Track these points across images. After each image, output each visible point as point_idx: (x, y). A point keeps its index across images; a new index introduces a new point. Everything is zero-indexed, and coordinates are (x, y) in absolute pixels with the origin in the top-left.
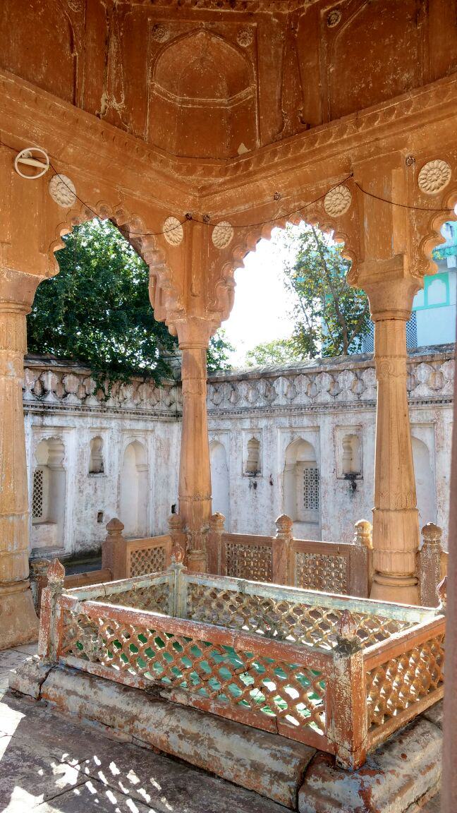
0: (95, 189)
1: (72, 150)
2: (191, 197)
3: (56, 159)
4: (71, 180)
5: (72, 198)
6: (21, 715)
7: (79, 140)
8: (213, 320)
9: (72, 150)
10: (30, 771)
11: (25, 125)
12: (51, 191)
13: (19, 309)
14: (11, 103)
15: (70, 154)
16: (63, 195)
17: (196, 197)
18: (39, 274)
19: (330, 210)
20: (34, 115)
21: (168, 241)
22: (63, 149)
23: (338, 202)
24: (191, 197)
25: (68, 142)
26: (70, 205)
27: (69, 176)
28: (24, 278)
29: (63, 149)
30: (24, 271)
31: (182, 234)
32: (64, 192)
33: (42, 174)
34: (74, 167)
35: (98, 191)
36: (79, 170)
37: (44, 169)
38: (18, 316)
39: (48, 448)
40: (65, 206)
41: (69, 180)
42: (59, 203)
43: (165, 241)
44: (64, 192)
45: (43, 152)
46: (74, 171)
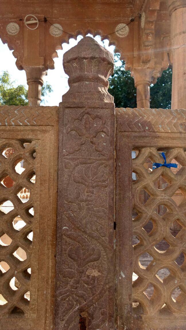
0: (74, 25)
2: (129, 9)
4: (60, 24)
5: (61, 32)
8: (148, 68)
9: (56, 11)
10: (47, 326)
12: (50, 32)
16: (12, 30)
17: (132, 7)
18: (39, 66)
19: (8, 29)
21: (119, 36)
23: (13, 29)
24: (129, 9)
26: (59, 35)
28: (33, 69)
31: (128, 30)
35: (75, 25)
36: (64, 19)
40: (57, 36)
41: (59, 25)
42: (54, 36)
43: (117, 36)
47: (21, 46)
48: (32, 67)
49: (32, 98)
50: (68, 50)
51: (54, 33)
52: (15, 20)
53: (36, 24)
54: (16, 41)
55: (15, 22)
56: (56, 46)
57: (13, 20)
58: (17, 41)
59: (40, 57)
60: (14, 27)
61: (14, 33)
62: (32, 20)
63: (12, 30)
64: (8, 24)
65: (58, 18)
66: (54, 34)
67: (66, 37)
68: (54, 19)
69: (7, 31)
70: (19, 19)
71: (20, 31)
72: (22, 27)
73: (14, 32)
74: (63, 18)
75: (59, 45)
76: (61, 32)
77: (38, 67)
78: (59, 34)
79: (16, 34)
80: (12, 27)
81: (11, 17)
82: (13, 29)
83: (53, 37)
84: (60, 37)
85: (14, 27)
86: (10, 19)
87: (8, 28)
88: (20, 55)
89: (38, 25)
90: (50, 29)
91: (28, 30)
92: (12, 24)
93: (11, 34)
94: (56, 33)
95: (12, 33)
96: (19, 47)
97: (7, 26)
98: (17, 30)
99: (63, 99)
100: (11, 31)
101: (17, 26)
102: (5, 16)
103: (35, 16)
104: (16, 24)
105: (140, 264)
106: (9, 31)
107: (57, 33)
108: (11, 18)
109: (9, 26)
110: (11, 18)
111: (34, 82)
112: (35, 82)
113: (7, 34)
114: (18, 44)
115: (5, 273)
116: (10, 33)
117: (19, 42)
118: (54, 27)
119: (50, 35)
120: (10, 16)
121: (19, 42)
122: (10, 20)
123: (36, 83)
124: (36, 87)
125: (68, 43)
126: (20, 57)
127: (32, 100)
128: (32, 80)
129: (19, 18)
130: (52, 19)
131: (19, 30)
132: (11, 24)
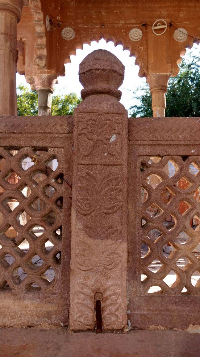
1: (182, 15)
3: (176, 22)
4: (185, 29)
5: (185, 37)
6: (65, 65)
7: (184, 9)
11: (158, 13)
12: (174, 37)
13: (159, 89)
14: (149, 7)
15: (182, 17)
18: (167, 73)
20: (160, 7)
22: (178, 16)
23: (136, 35)
25: (179, 12)
26: (184, 40)
27: (183, 27)
28: (160, 76)
29: (178, 16)
30: (160, 73)
32: (181, 35)
33: (165, 30)
34: (186, 22)
36: (189, 22)
37: (154, 27)
38: (159, 92)
39: (138, 106)
40: (181, 41)
42: (178, 41)
44: (181, 35)
45: (164, 21)
46: (186, 24)
47: (144, 53)
48: (160, 75)
49: (159, 106)
50: (114, 54)
51: (178, 37)
52: (137, 26)
53: (163, 29)
54: (139, 47)
55: (138, 28)
56: (181, 51)
57: (135, 26)
58: (140, 48)
59: (167, 64)
60: (137, 33)
61: (137, 39)
62: (159, 25)
63: (180, 37)
64: (131, 30)
65: (183, 22)
66: (178, 40)
67: (190, 41)
68: (178, 24)
69: (130, 37)
70: (141, 24)
71: (143, 37)
72: (145, 33)
73: (136, 38)
74: (188, 22)
75: (183, 51)
76: (185, 37)
77: (166, 74)
78: (184, 39)
79: (139, 40)
80: (135, 33)
81: (134, 23)
82: (136, 35)
83: (177, 42)
84: (185, 42)
85: (137, 33)
86: (133, 25)
87: (131, 34)
88: (144, 61)
89: (165, 30)
90: (174, 34)
91: (153, 35)
92: (134, 30)
93: (134, 40)
94: (180, 38)
95: (135, 40)
96: (142, 53)
97: (129, 32)
98: (140, 36)
99: (121, 105)
100: (134, 37)
101: (140, 32)
102: (128, 22)
103: (166, 21)
104: (139, 30)
105: (160, 262)
106: (132, 37)
107: (182, 38)
108: (133, 24)
109: (132, 32)
110: (133, 24)
111: (159, 90)
112: (161, 89)
113: (130, 40)
114: (141, 50)
115: (51, 282)
116: (133, 39)
117: (142, 48)
118: (178, 31)
119: (174, 40)
120: (133, 21)
121: (142, 48)
122: (132, 26)
123: (162, 91)
124: (162, 95)
125: (116, 45)
126: (144, 64)
127: (158, 109)
128: (159, 88)
129: (142, 23)
130: (176, 23)
131: (142, 36)
132: (134, 30)
